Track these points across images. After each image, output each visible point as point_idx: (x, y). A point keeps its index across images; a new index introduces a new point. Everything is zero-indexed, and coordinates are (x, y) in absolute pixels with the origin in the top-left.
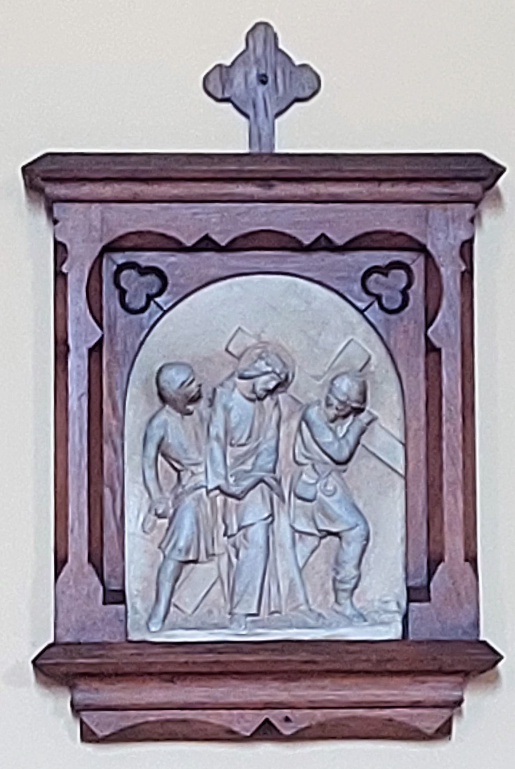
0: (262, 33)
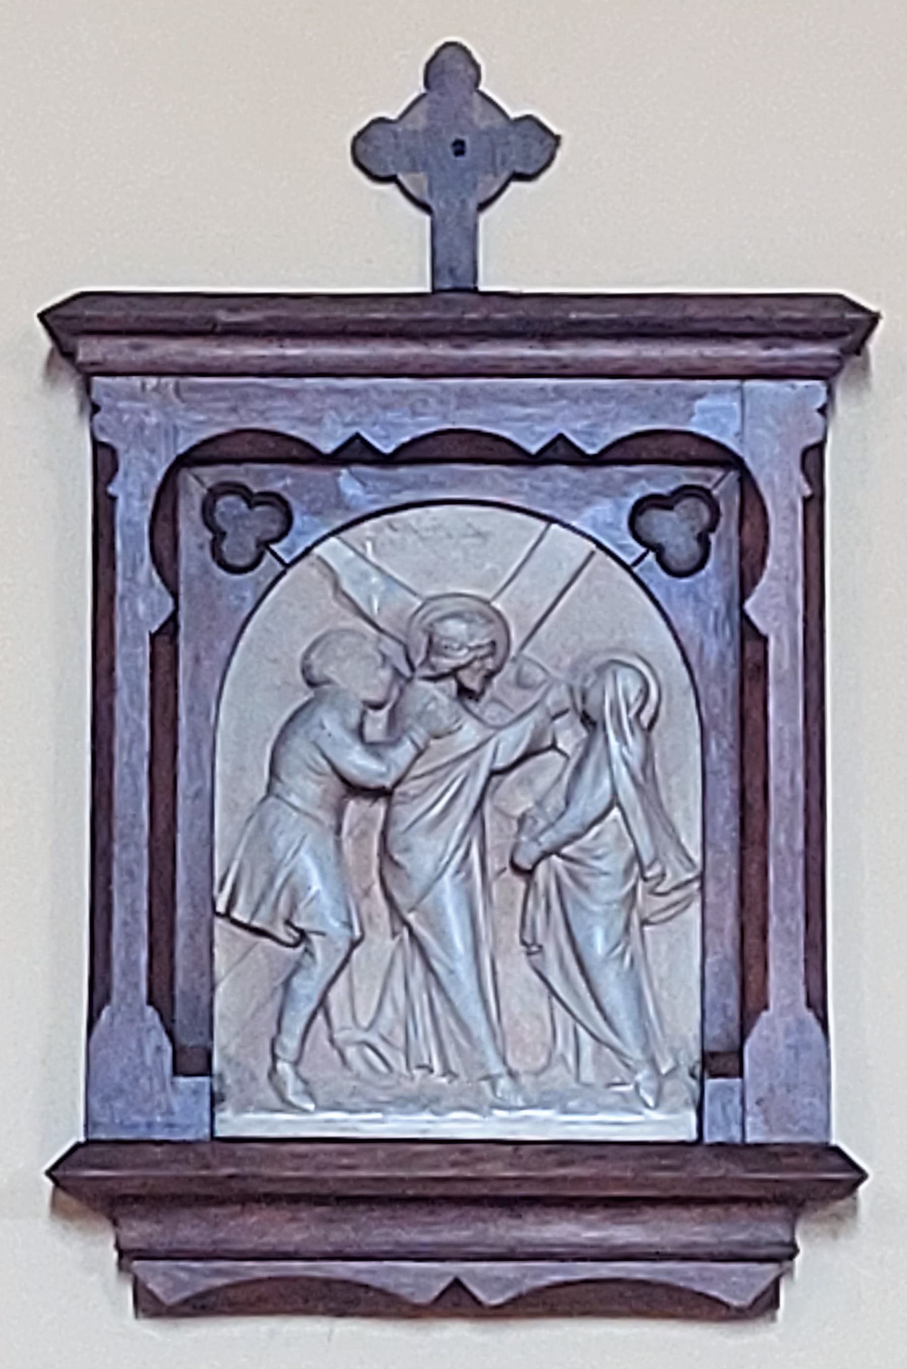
0: (450, 69)
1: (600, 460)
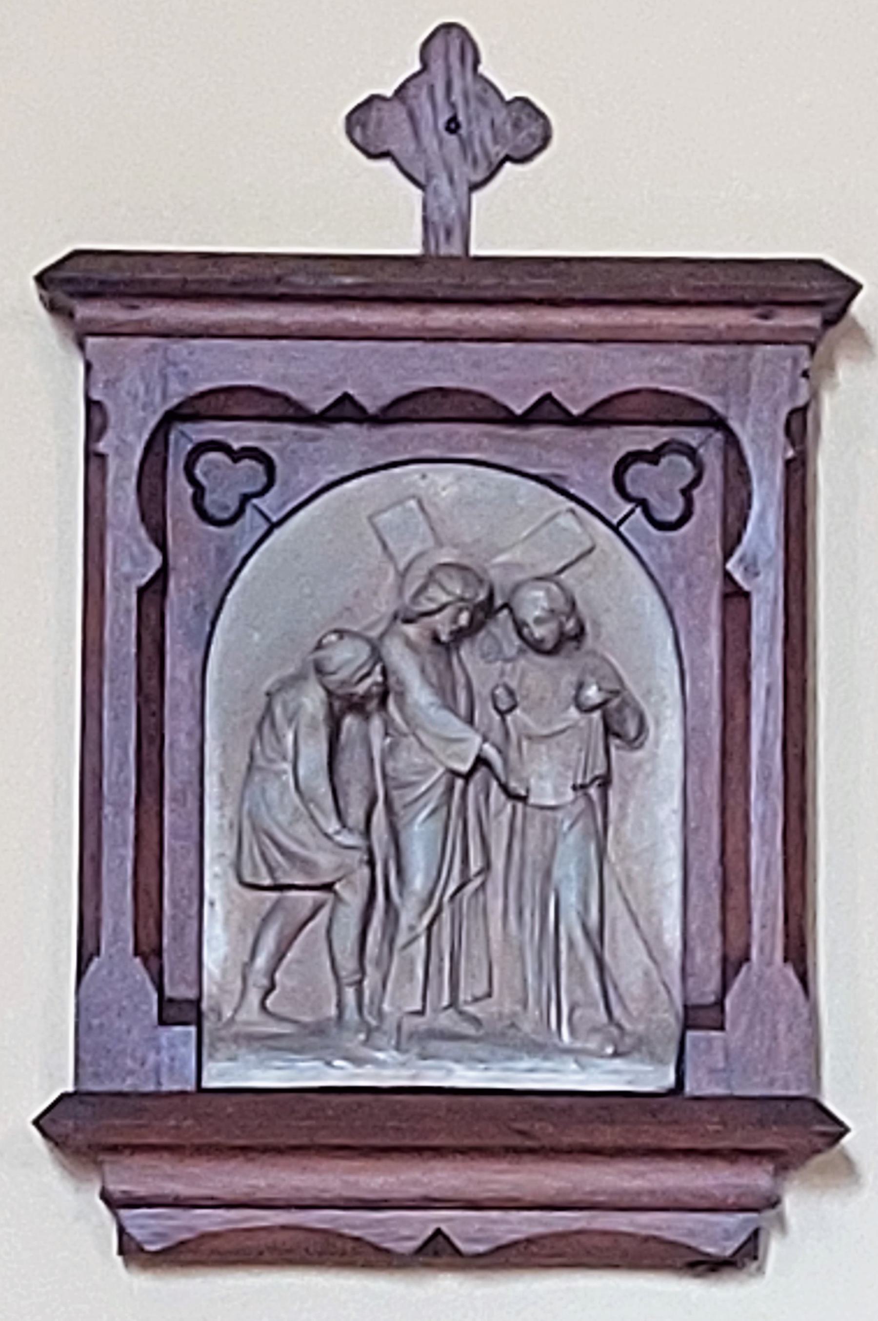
0: (451, 43)
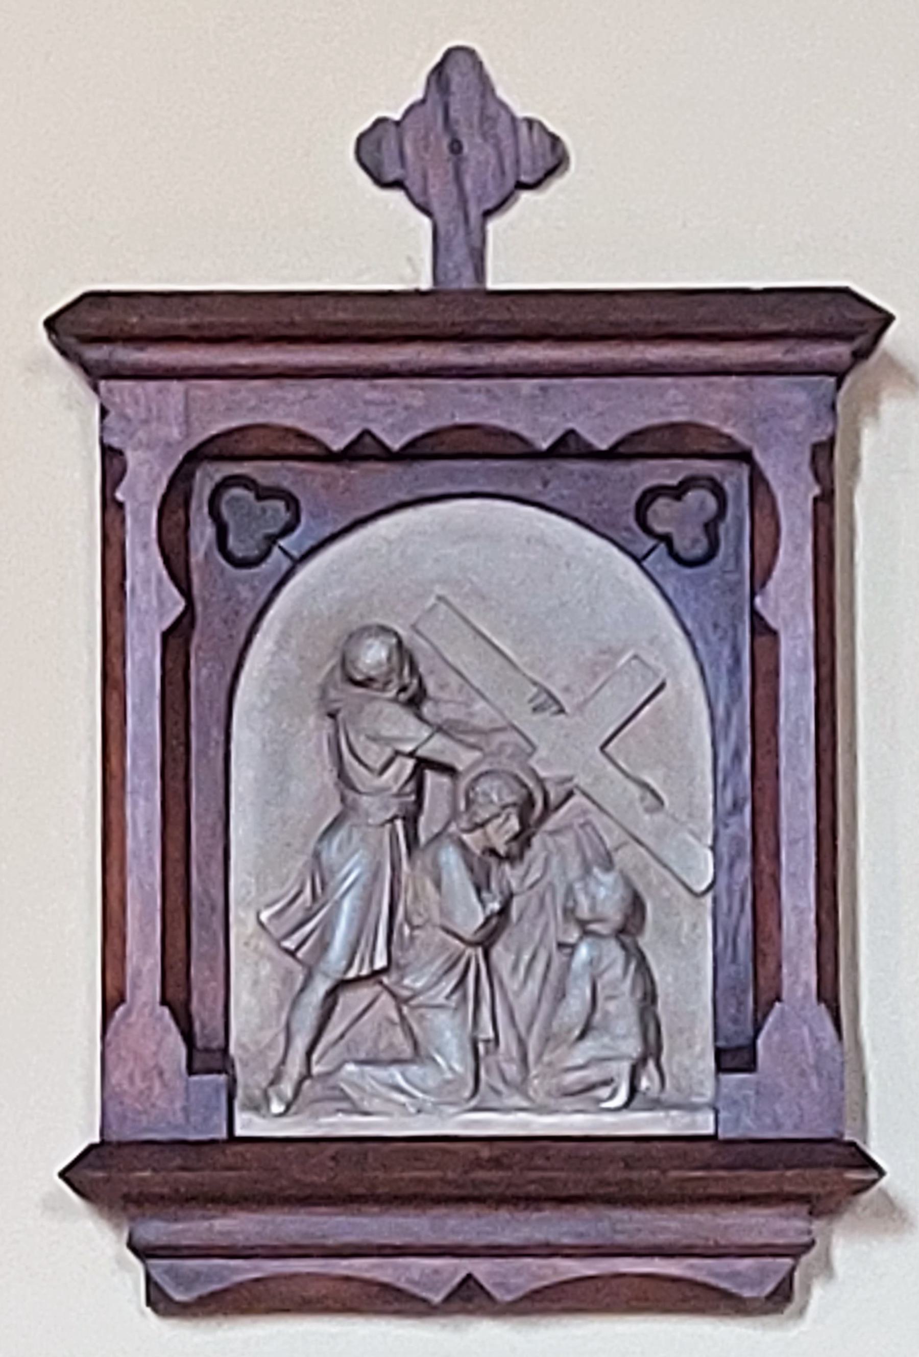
0: (456, 75)
1: (612, 455)
